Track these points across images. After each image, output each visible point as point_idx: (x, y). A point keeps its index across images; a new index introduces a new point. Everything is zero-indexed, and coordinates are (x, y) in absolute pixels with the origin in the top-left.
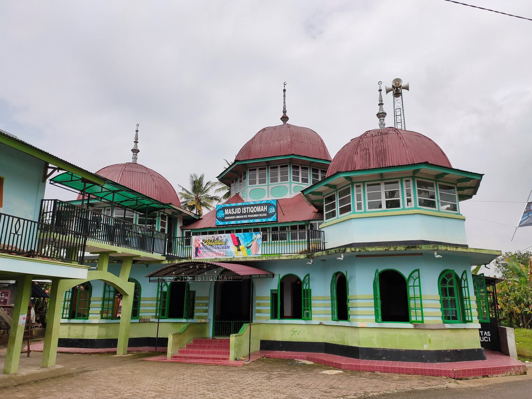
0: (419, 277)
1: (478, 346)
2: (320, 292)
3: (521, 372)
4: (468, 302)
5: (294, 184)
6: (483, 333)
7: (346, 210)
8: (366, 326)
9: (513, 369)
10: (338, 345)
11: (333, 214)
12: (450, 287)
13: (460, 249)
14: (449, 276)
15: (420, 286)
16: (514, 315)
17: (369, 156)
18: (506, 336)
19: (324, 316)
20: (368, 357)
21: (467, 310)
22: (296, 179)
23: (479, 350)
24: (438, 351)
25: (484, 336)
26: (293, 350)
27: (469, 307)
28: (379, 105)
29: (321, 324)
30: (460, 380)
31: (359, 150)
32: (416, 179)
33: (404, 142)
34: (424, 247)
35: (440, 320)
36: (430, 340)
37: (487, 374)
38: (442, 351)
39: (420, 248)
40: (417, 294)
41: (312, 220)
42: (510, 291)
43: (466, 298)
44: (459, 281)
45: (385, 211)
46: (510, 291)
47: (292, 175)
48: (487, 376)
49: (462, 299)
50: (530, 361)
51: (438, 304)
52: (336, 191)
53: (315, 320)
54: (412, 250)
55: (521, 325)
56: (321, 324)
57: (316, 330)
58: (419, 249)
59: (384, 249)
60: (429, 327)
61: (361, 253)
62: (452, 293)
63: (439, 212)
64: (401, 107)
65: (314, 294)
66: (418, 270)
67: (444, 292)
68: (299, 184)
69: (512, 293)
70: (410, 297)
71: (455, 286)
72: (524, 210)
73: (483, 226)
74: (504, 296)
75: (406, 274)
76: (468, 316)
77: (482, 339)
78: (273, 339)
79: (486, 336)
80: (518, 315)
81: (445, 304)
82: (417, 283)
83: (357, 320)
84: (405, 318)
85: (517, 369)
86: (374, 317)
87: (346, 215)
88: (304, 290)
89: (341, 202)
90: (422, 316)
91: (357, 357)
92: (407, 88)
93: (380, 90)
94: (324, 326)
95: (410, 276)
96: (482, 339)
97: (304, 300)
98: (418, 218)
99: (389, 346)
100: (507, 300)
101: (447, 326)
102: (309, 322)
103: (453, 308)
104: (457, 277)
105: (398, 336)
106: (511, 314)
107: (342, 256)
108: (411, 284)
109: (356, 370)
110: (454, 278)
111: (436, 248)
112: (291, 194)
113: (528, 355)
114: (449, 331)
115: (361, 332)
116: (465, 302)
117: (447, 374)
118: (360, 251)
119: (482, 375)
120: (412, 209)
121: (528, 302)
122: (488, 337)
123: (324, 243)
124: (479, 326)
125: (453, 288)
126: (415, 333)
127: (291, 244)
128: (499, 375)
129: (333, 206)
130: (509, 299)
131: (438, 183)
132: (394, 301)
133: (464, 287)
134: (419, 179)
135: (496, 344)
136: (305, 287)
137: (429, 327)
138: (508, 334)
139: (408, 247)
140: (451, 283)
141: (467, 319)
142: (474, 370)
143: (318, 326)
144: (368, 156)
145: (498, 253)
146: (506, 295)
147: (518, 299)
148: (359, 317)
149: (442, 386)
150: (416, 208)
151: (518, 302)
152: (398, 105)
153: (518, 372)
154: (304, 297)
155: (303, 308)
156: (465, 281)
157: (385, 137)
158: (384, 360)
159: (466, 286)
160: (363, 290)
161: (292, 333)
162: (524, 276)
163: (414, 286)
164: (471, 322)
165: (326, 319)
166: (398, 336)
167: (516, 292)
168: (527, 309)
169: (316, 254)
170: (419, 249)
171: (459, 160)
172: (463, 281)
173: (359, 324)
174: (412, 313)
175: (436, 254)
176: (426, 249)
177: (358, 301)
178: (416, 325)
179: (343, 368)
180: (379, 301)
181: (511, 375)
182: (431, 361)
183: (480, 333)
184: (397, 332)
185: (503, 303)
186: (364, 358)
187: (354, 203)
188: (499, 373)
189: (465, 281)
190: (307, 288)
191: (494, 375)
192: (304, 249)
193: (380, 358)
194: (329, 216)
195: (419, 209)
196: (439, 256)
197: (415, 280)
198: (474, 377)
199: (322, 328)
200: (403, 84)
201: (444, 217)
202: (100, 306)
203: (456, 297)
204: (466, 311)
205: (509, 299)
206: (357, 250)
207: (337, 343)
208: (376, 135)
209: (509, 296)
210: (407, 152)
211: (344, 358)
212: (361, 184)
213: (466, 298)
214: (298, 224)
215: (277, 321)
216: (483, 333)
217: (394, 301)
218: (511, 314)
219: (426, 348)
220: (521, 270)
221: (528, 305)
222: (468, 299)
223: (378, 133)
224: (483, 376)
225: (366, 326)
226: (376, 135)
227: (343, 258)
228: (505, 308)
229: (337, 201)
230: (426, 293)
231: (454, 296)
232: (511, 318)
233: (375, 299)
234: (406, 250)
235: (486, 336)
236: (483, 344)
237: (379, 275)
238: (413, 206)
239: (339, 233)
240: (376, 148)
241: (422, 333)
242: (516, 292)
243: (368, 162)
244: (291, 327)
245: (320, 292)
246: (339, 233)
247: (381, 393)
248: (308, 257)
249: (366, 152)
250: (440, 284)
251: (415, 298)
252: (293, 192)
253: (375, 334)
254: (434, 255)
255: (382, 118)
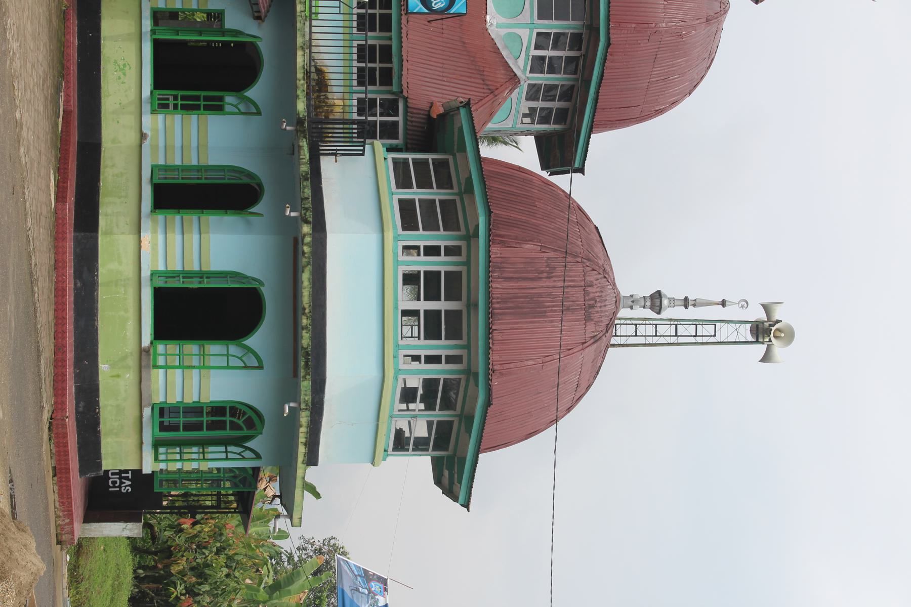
0: (246, 367)
1: (108, 464)
2: (216, 139)
3: (61, 535)
4: (195, 456)
5: (528, 36)
6: (127, 478)
7: (408, 216)
8: (142, 251)
9: (67, 521)
10: (98, 180)
11: (403, 182)
12: (224, 422)
13: (302, 450)
14: (250, 424)
15: (228, 367)
16: (166, 561)
17: (532, 279)
18: (126, 521)
19: (161, 144)
20: (78, 250)
21: (180, 453)
22: (542, 40)
23: (99, 465)
24: (97, 390)
25: (121, 478)
26: (80, 66)
27: (186, 456)
28: (686, 299)
29: (143, 136)
30: (49, 428)
31: (551, 254)
32: (462, 377)
33: (575, 350)
34: (306, 385)
35: (159, 398)
36: (118, 376)
37: (59, 475)
38: (98, 396)
39: (304, 377)
40: (213, 361)
41: (406, 107)
42: (229, 558)
43: (203, 453)
44: (238, 442)
45: (396, 308)
46: (229, 558)
47: (553, 31)
48: (54, 475)
49: (203, 443)
50: (70, 563)
51: (192, 398)
52: (460, 194)
53: (153, 122)
54: (305, 361)
55: (141, 571)
56: (143, 136)
57: (129, 120)
58: (302, 374)
59: (306, 306)
60: (145, 382)
61: (303, 252)
62: (212, 426)
63: (391, 417)
64: (718, 339)
65: (213, 121)
66: (260, 367)
67: (218, 410)
68: (528, 49)
69: (222, 559)
70: (207, 347)
71: (228, 433)
72: (372, 570)
73: (360, 497)
74: (216, 541)
75: (253, 341)
76: (167, 453)
77: (113, 474)
78: (103, 9)
79: (121, 483)
80: (167, 567)
81: (195, 410)
82: (234, 362)
83: (154, 232)
84: (162, 332)
85: (67, 528)
86: (161, 267)
87: (394, 216)
88: (221, 99)
89: (429, 205)
90: (166, 367)
91: (78, 228)
92: (766, 358)
93: (723, 303)
94: (138, 142)
95: (249, 350)
96: (113, 474)
97: (197, 98)
98: (373, 372)
99: (103, 295)
100: (206, 548)
101: (147, 412)
102: (146, 108)
103: (181, 424)
104: (249, 438)
105: (124, 319)
106: (168, 553)
107: (293, 214)
108: (233, 349)
109: (58, 236)
110: (245, 432)
111: (303, 406)
112: (499, 26)
113: (82, 562)
114: (137, 413)
115: (130, 239)
116: (195, 449)
117: (60, 406)
118: (304, 253)
119: (58, 467)
120: (396, 364)
121: (198, 594)
122: (120, 487)
123: (335, 155)
124: (147, 470)
125: (225, 429)
126: (130, 347)
127: (347, 43)
128: (57, 495)
129: (424, 183)
130: (207, 552)
131: (456, 420)
132: (193, 312)
133: (226, 452)
134: (463, 384)
135: (107, 499)
136: (230, 99)
137: (145, 382)
138: (130, 525)
139: (307, 354)
140: (235, 426)
141: (162, 450)
142: (66, 454)
143: (141, 131)
144: (530, 275)
145: (296, 520)
146: (218, 545)
147: (207, 571)
148: (161, 237)
149: (44, 399)
150: (398, 372)
151: (201, 572)
152: (725, 332)
153: (62, 529)
154: (206, 98)
155: (180, 93)
156: (239, 454)
157: (580, 314)
158: (75, 284)
159: (230, 456)
160: (222, 248)
161: (121, 63)
162: (271, 598)
163: (228, 355)
164: (156, 459)
165: (154, 148)
166: (124, 319)
167: (225, 571)
168: (180, 588)
169: (304, 144)
170: (302, 374)
171: (492, 467)
172: (238, 450)
173: (146, 237)
174: (173, 347)
175: (292, 405)
176: (303, 389)
177: (196, 237)
178: (147, 351)
179: (60, 207)
180: (194, 284)
181: (57, 517)
182: (77, 377)
183: (126, 471)
184: (131, 314)
185: (196, 536)
186: (77, 241)
187: (422, 238)
188: (61, 495)
189: (239, 454)
190: (228, 108)
191: (56, 488)
192: (333, 83)
193: (78, 275)
194: (401, 169)
195: (396, 379)
196: (287, 411)
197: (240, 358)
198: (54, 451)
199: (133, 137)
200: (778, 349)
201: (377, 426)
202: (186, 163)
203: (205, 433)
204: (178, 450)
205: (207, 552)
206: (306, 249)
207: (102, 177)
208: (586, 293)
209: (218, 552)
210: (530, 363)
211: (73, 206)
212: (462, 259)
213: (203, 453)
214: (395, 65)
215: (147, 24)
216: (127, 478)
217: (193, 312)
218: (168, 553)
219: (103, 367)
220: (289, 592)
221: (191, 592)
222: (201, 455)
223: (593, 299)
224: (54, 468)
225: (142, 251)
226: (586, 293)
227: (289, 216)
228: (183, 538)
229: (435, 194)
230: (211, 376)
231: (209, 428)
232: (155, 553)
233: (201, 275)
234: (303, 348)
235: (121, 483)
236: (107, 472)
237: (255, 289)
238: (402, 367)
239: (356, 191)
240: (550, 294)
241: (132, 362)
242: (225, 571)
243: (516, 275)
244: (133, 60)
245: (216, 139)
246: (356, 191)
247: (38, 305)
248: (300, 122)
249: (542, 272)
250: (233, 405)
251: (203, 355)
252: (503, 32)
253: (128, 269)
254: (288, 402)
255: (648, 304)
